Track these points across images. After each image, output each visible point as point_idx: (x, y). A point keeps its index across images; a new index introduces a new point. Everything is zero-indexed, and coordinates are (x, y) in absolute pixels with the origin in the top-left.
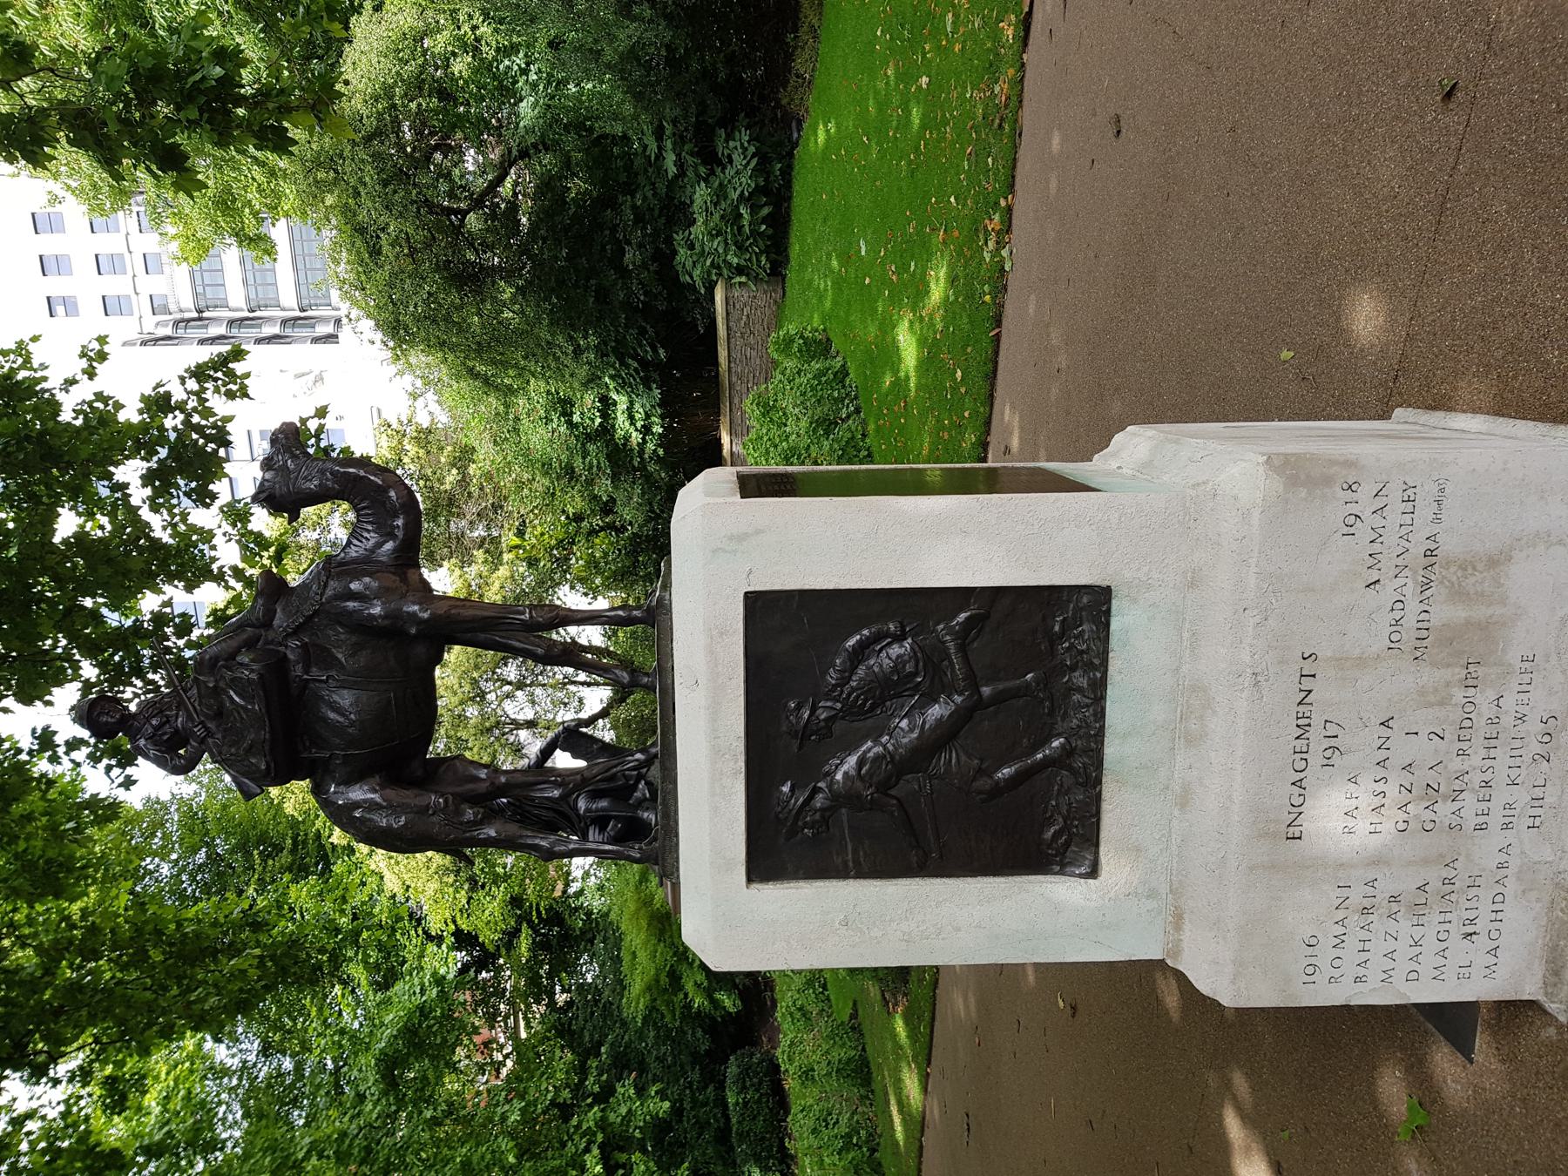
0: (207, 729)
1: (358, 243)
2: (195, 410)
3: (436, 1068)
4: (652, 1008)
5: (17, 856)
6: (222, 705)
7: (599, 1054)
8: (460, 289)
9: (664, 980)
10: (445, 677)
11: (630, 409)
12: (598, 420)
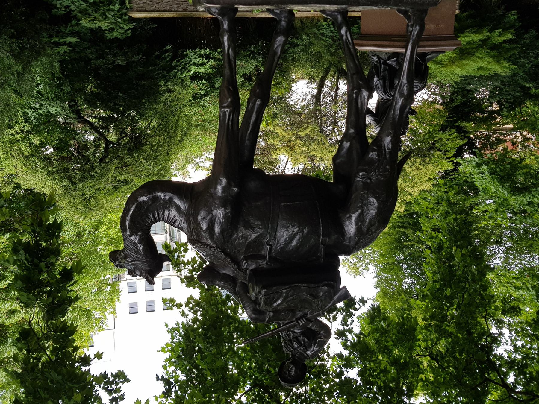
0: (301, 317)
1: (122, 189)
2: (192, 266)
3: (522, 168)
4: (508, 60)
5: (395, 345)
6: (284, 310)
7: (529, 88)
8: (143, 145)
9: (494, 53)
10: (288, 165)
11: (198, 65)
12: (204, 81)
